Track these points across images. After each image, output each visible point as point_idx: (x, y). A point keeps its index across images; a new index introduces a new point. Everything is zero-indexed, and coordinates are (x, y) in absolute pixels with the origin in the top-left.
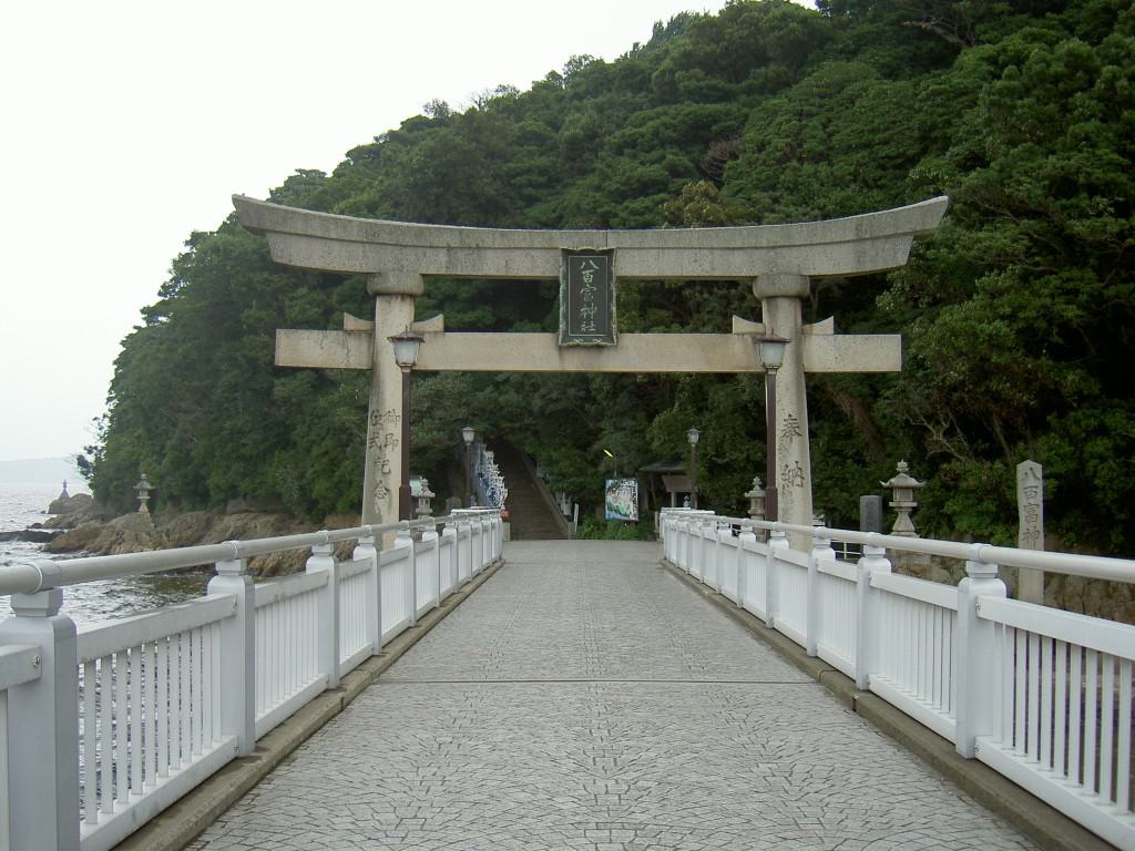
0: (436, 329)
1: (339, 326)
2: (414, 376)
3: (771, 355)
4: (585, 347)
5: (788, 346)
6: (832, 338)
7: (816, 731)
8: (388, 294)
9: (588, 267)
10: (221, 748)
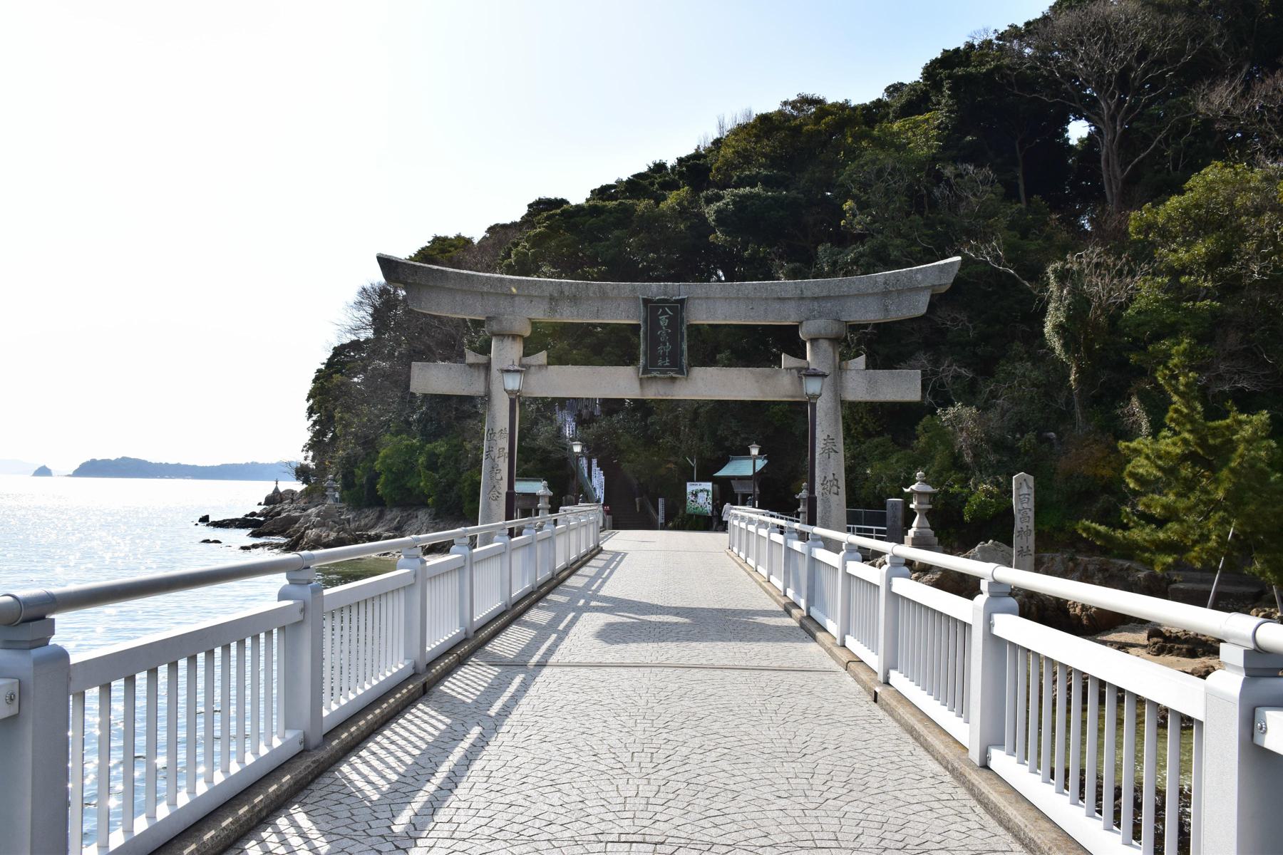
0: (540, 363)
1: (461, 356)
2: (516, 400)
3: (813, 386)
4: (660, 378)
5: (826, 379)
6: (863, 373)
7: (839, 724)
8: (502, 336)
9: (664, 313)
10: (293, 738)
